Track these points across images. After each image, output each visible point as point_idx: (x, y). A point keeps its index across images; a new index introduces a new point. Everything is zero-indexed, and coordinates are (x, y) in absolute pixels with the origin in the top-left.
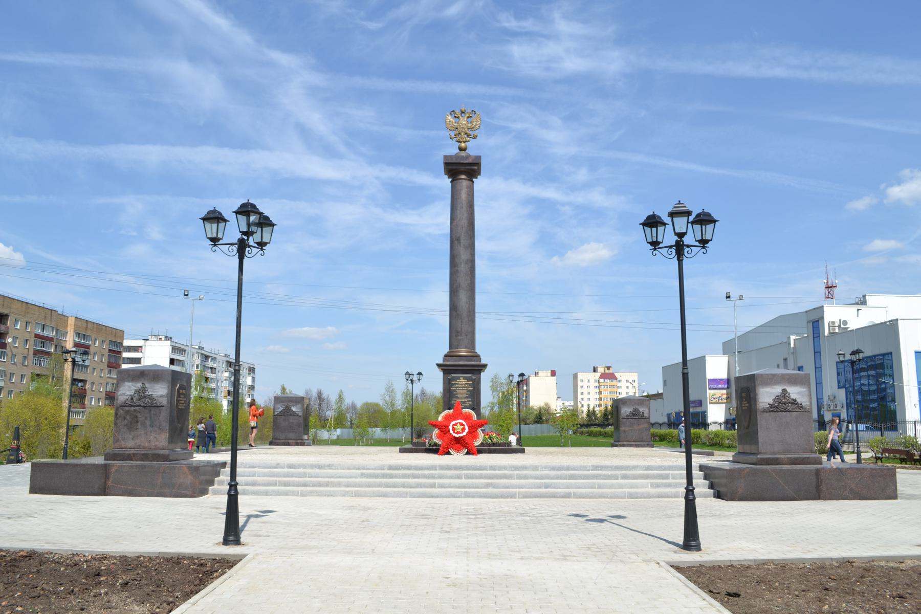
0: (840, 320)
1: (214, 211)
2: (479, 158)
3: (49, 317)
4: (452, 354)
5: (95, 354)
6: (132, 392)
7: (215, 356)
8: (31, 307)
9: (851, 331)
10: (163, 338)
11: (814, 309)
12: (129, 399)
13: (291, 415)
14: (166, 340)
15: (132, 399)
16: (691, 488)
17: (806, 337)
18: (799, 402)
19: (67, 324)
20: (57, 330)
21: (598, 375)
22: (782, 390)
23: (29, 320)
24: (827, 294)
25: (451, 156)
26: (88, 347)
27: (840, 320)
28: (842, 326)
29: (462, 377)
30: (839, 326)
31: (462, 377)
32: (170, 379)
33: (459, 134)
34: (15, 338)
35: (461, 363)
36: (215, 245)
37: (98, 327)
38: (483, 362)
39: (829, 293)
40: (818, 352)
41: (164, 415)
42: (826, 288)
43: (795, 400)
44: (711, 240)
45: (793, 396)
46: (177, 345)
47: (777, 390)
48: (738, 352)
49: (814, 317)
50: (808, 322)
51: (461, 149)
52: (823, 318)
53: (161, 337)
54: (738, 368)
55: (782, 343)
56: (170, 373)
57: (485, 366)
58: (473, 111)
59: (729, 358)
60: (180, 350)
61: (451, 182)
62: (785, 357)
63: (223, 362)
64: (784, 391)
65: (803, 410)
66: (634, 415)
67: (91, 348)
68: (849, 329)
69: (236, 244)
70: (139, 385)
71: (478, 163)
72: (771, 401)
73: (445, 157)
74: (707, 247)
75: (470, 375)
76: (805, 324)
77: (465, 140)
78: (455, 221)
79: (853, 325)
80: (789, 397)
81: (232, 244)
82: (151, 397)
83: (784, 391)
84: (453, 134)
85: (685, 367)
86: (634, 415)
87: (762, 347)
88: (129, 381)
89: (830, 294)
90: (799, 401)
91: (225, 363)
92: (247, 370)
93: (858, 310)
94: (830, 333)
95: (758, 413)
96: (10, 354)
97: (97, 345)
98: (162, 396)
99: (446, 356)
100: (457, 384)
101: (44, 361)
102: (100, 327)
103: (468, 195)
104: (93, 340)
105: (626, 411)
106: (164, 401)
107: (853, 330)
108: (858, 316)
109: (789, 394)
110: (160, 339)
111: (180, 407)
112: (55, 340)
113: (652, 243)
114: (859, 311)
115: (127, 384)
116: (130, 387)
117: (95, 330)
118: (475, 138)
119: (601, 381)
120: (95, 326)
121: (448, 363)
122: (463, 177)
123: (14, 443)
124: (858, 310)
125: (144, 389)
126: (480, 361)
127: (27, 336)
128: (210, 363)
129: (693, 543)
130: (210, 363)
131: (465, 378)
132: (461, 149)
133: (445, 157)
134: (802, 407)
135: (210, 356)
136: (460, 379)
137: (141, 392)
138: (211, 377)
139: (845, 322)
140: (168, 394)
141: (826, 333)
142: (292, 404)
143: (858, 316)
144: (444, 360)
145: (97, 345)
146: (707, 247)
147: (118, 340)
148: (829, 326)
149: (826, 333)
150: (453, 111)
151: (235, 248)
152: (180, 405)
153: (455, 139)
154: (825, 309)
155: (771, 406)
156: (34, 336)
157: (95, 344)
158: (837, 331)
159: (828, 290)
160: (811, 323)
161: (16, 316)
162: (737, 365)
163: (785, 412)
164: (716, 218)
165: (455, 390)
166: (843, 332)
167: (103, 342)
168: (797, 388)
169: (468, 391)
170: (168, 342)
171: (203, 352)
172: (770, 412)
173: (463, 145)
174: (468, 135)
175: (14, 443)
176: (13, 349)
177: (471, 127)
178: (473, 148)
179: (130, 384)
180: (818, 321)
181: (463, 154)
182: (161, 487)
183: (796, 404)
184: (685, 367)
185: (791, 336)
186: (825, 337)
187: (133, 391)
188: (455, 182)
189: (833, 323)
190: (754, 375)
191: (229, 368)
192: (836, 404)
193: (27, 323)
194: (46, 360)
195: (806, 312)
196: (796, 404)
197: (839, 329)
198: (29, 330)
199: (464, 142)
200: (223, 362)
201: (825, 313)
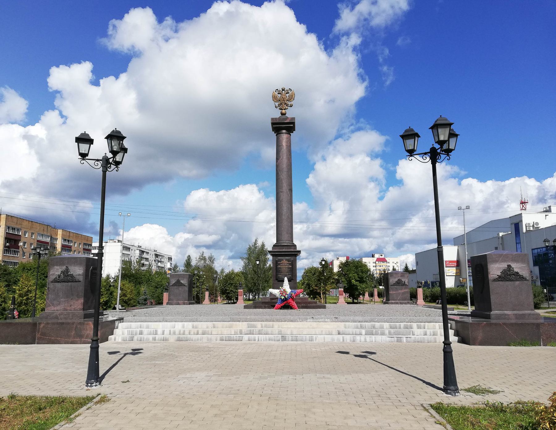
0: (534, 222)
1: (85, 134)
2: (294, 119)
3: (46, 230)
4: (279, 244)
5: (75, 251)
6: (59, 273)
7: (148, 251)
8: (34, 224)
9: (541, 229)
10: (117, 241)
11: (515, 215)
12: (57, 277)
13: (180, 286)
14: (119, 242)
15: (59, 277)
16: (447, 342)
17: (510, 233)
18: (521, 274)
19: (57, 233)
20: (51, 237)
21: (375, 259)
22: (508, 266)
23: (33, 232)
24: (522, 207)
25: (276, 119)
26: (70, 247)
27: (534, 222)
28: (535, 226)
29: (284, 259)
30: (533, 226)
31: (284, 259)
32: (85, 264)
33: (281, 104)
34: (25, 243)
35: (284, 250)
36: (83, 159)
37: (76, 235)
38: (298, 249)
39: (523, 206)
40: (519, 243)
41: (81, 287)
42: (521, 203)
43: (518, 273)
44: (454, 150)
45: (516, 270)
46: (125, 245)
47: (504, 265)
48: (324, 337)
49: (516, 221)
50: (511, 224)
51: (282, 114)
52: (521, 221)
53: (115, 240)
54: (467, 253)
55: (494, 238)
56: (85, 259)
57: (299, 252)
58: (289, 89)
59: (458, 248)
60: (125, 248)
61: (276, 135)
62: (496, 246)
63: (153, 255)
64: (509, 266)
65: (524, 280)
66: (398, 283)
67: (72, 248)
68: (540, 228)
69: (101, 160)
70: (64, 268)
71: (293, 122)
72: (499, 274)
73: (272, 119)
74: (450, 155)
75: (290, 258)
76: (509, 225)
77: (285, 108)
78: (279, 160)
79: (542, 225)
80: (513, 271)
81: (98, 160)
82: (72, 276)
83: (509, 266)
84: (277, 104)
85: (440, 246)
86: (398, 283)
87: (480, 240)
88: (57, 265)
89: (523, 207)
90: (520, 273)
91: (154, 255)
92: (167, 259)
93: (546, 215)
94: (527, 231)
95: (490, 282)
96: (21, 252)
97: (76, 246)
98: (79, 275)
99: (274, 246)
100: (282, 263)
101: (43, 257)
102: (78, 235)
103: (287, 143)
104: (74, 242)
105: (392, 281)
106: (81, 278)
107: (543, 228)
108: (546, 219)
109: (513, 269)
110: (115, 242)
111: (92, 282)
112: (49, 244)
113: (408, 151)
114: (547, 216)
115: (56, 267)
116: (57, 269)
117: (75, 237)
118: (291, 107)
119: (377, 262)
120: (75, 235)
121: (276, 250)
122: (284, 131)
123: (12, 307)
124: (546, 215)
125: (67, 270)
126: (296, 249)
127: (32, 241)
128: (145, 255)
129: (452, 388)
130: (145, 255)
131: (286, 260)
132: (282, 114)
133: (272, 119)
134: (523, 278)
135: (145, 251)
136: (283, 261)
137: (66, 272)
138: (146, 264)
139: (537, 224)
140: (83, 273)
141: (524, 231)
142: (181, 278)
143: (546, 219)
144: (273, 248)
145: (76, 246)
146: (450, 155)
147: (89, 243)
148: (526, 227)
149: (524, 231)
150: (277, 89)
151: (100, 164)
152: (93, 280)
153: (278, 108)
154: (523, 215)
155: (500, 277)
156: (36, 241)
157: (75, 245)
158: (532, 229)
159: (522, 205)
160: (514, 224)
161: (25, 230)
162: (466, 251)
163: (510, 281)
164: (457, 133)
165: (280, 267)
166: (536, 230)
167: (80, 244)
168: (518, 264)
169: (288, 268)
170: (120, 244)
171: (141, 249)
172: (499, 281)
173: (284, 111)
174: (287, 105)
175: (12, 307)
176: (24, 249)
177: (289, 100)
178: (290, 113)
179: (58, 267)
180: (518, 223)
181: (284, 117)
182: (74, 337)
183: (518, 276)
184: (440, 246)
185: (500, 233)
186: (523, 233)
187: (60, 272)
188: (279, 135)
189: (529, 224)
190: (486, 254)
191: (157, 258)
192: (532, 276)
193: (32, 233)
194: (44, 255)
195: (510, 217)
196: (518, 276)
197: (533, 228)
198: (33, 238)
199: (284, 109)
200: (153, 255)
201: (523, 218)
